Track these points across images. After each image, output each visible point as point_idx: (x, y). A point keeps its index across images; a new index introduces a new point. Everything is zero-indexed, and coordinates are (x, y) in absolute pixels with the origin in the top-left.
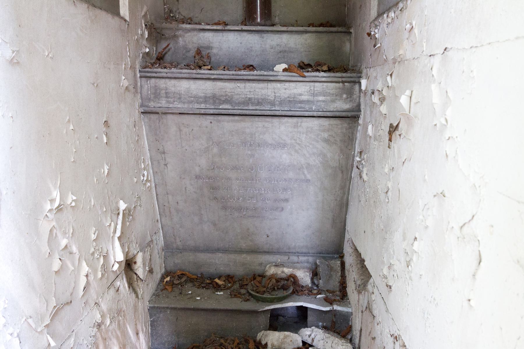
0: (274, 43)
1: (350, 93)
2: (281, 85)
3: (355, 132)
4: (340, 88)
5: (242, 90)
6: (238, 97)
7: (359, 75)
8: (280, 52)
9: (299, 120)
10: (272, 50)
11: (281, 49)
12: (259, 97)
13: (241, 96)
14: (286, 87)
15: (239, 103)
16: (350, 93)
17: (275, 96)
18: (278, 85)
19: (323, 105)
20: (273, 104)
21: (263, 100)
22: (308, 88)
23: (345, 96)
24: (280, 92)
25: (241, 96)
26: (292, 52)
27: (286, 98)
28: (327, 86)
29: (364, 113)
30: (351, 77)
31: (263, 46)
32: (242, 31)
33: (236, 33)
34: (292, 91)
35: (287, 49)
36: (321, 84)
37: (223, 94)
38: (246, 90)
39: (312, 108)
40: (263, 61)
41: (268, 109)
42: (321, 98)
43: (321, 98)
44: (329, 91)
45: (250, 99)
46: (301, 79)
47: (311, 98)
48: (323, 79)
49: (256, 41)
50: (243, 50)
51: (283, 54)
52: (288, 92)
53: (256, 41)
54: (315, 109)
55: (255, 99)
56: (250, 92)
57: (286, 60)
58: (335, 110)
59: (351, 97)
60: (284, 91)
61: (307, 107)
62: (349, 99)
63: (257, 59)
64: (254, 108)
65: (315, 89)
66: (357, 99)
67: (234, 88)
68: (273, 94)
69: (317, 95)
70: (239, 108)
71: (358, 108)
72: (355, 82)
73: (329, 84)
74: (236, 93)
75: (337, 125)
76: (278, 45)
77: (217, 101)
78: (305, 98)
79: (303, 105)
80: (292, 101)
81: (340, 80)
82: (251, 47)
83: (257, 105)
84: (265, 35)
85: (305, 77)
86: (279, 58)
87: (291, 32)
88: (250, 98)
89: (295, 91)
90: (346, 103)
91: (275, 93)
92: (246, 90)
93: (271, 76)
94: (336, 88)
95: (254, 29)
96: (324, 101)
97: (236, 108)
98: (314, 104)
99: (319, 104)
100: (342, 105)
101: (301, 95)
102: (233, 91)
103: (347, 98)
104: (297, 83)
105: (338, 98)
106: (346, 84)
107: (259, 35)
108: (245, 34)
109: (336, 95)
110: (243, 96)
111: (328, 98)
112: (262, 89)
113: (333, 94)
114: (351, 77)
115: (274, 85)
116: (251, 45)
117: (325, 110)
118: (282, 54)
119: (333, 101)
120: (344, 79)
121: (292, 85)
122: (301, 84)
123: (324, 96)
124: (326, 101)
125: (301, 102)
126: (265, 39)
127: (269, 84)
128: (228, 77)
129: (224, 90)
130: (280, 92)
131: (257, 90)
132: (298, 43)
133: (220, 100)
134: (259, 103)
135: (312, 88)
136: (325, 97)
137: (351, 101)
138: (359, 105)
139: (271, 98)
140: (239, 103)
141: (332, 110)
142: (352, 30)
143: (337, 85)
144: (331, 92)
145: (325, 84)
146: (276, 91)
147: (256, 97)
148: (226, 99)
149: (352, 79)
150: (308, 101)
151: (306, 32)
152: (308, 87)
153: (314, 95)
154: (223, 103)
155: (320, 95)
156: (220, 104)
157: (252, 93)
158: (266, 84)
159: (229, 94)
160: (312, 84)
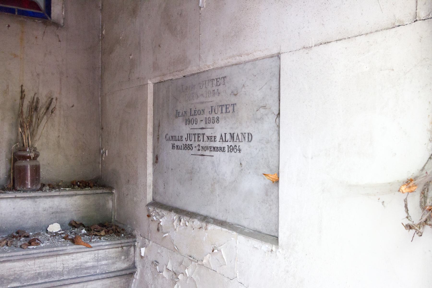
0: (47, 206)
1: (127, 254)
2: (69, 256)
3: (130, 284)
4: (119, 252)
5: (31, 267)
6: (27, 273)
7: (134, 240)
8: (52, 213)
9: (86, 284)
10: (45, 212)
11: (54, 210)
12: (49, 270)
13: (30, 272)
14: (73, 257)
15: (29, 280)
16: (127, 254)
17: (63, 267)
18: (67, 257)
19: (105, 268)
20: (61, 274)
21: (52, 272)
22: (92, 256)
23: (123, 257)
24: (68, 263)
25: (30, 272)
26: (63, 212)
27: (73, 267)
28: (109, 252)
29: (142, 273)
30: (128, 242)
31: (36, 209)
32: (16, 197)
33: (9, 200)
34: (79, 261)
35: (59, 210)
36: (104, 251)
37: (12, 273)
38: (36, 266)
39: (96, 272)
40: (36, 223)
41: (57, 279)
42: (104, 262)
43: (104, 262)
44: (110, 256)
45: (39, 274)
46: (88, 249)
47: (96, 264)
48: (106, 247)
49: (29, 206)
50: (16, 215)
51: (55, 215)
52: (75, 261)
53: (29, 206)
54: (99, 272)
55: (44, 273)
56: (39, 267)
57: (58, 219)
58: (115, 270)
59: (128, 257)
60: (72, 261)
61: (92, 272)
62: (126, 260)
63: (30, 222)
64: (43, 281)
65: (99, 256)
66: (133, 258)
67: (23, 266)
68: (62, 266)
69: (100, 260)
70: (28, 283)
71: (134, 266)
72: (131, 246)
73: (111, 250)
74: (25, 270)
75: (117, 282)
76: (50, 207)
77: (5, 281)
78: (90, 264)
79: (88, 271)
80: (79, 269)
81: (120, 245)
82: (24, 211)
83: (46, 278)
84: (37, 200)
85: (91, 247)
86: (51, 218)
87: (63, 196)
88: (39, 273)
89: (82, 260)
90: (124, 263)
91: (63, 264)
92: (36, 266)
93: (60, 250)
94: (116, 252)
95: (28, 196)
96: (106, 265)
97: (25, 284)
98: (98, 268)
99: (102, 267)
100: (122, 265)
101: (87, 262)
102: (22, 269)
103: (125, 259)
104: (83, 253)
105: (118, 260)
106: (124, 248)
107: (33, 200)
108: (18, 200)
109: (116, 258)
110: (33, 272)
111: (110, 261)
112: (51, 262)
113: (113, 258)
114: (128, 242)
115: (63, 257)
116: (24, 210)
117: (107, 272)
118: (54, 214)
119: (114, 263)
120: (123, 245)
121: (79, 255)
122: (87, 253)
123: (107, 260)
124: (108, 264)
125: (87, 268)
126: (37, 203)
127: (58, 257)
128: (19, 258)
129: (13, 270)
130: (68, 263)
131: (46, 264)
132: (69, 204)
133: (9, 279)
134: (48, 276)
135: (97, 255)
136: (107, 261)
137: (128, 261)
138: (134, 263)
139: (60, 270)
140: (28, 279)
141: (113, 270)
142: (114, 191)
143: (117, 249)
144: (112, 256)
145: (107, 250)
146: (64, 262)
147: (46, 270)
148: (15, 278)
149: (129, 244)
150: (93, 267)
151: (76, 195)
152: (93, 255)
153: (98, 261)
154: (11, 283)
155: (103, 260)
156: (9, 283)
157: (41, 268)
158: (55, 258)
159: (18, 272)
160: (97, 252)
